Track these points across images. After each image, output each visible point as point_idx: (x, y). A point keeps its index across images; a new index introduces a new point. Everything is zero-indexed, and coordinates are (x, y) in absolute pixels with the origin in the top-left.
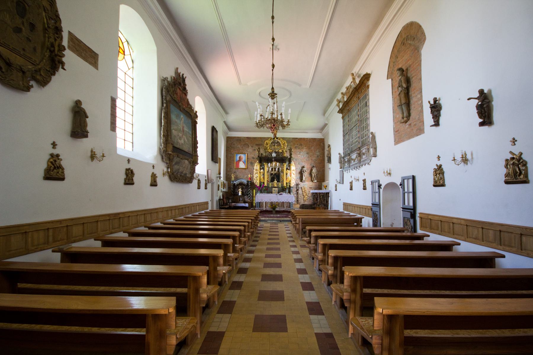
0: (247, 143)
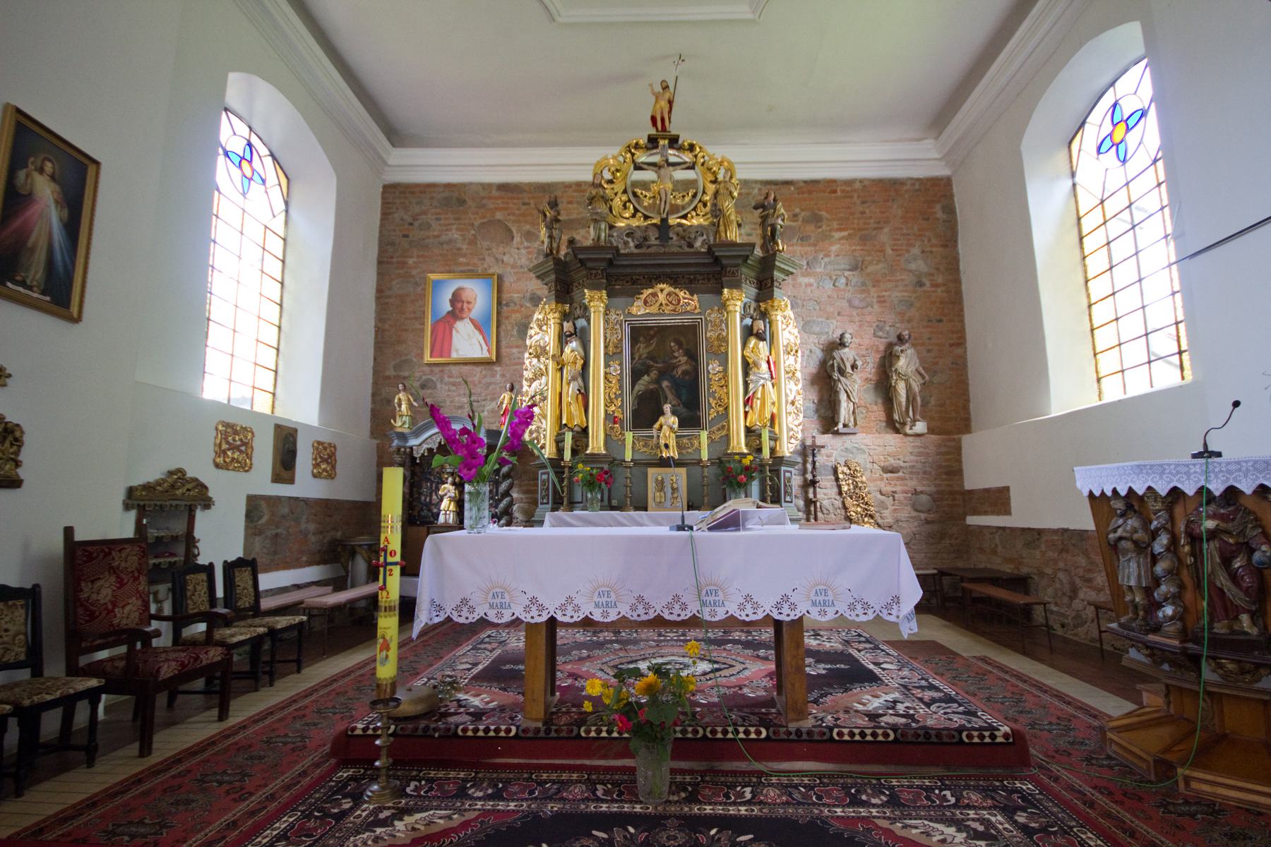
0: (499, 215)
